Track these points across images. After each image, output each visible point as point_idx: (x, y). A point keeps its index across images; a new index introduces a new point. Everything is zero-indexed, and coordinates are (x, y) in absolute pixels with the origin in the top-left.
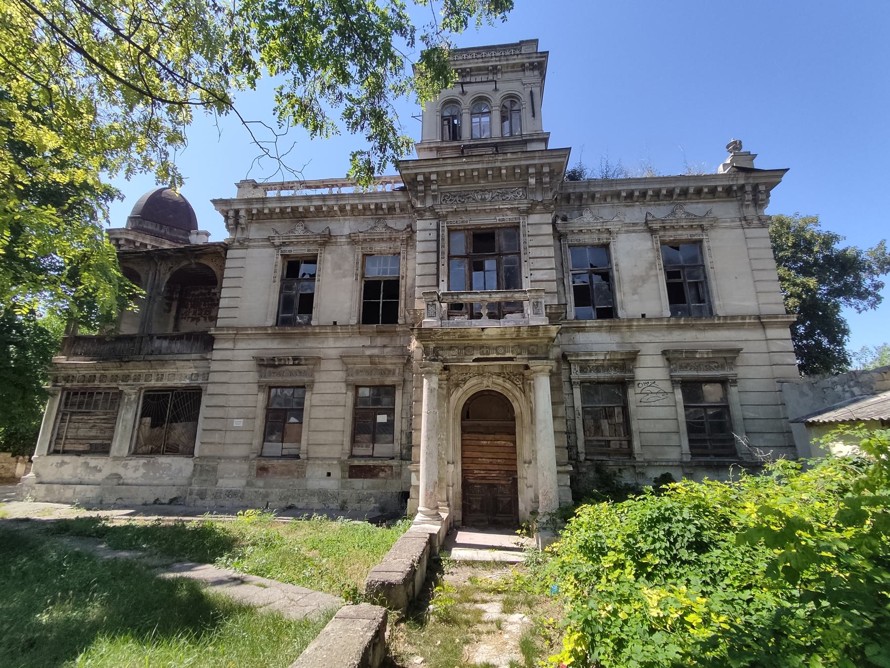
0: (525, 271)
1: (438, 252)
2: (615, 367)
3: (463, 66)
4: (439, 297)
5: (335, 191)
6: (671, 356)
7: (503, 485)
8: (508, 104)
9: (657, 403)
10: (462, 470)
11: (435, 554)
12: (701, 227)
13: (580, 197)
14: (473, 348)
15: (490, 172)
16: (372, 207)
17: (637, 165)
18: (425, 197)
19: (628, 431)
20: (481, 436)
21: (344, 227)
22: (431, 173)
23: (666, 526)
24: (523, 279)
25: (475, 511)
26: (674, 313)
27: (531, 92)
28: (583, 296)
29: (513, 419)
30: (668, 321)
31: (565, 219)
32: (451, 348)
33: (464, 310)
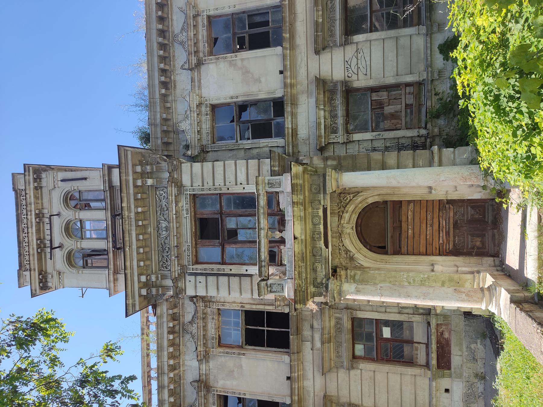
0: (238, 190)
1: (217, 275)
2: (331, 99)
3: (35, 247)
4: (263, 280)
5: (154, 374)
6: (320, 46)
7: (455, 214)
8: (73, 203)
9: (368, 59)
10: (440, 255)
11: (533, 298)
12: (195, 17)
13: (166, 132)
14: (314, 247)
15: (140, 223)
16: (171, 337)
17: (134, 73)
18: (162, 287)
19: (397, 86)
20: (404, 236)
21: (191, 366)
22: (139, 281)
23: (503, 101)
24: (245, 191)
25: (483, 243)
26: (279, 42)
27: (62, 181)
28: (262, 130)
29: (386, 202)
30: (286, 49)
31: (187, 147)
32: (314, 270)
33: (276, 250)
